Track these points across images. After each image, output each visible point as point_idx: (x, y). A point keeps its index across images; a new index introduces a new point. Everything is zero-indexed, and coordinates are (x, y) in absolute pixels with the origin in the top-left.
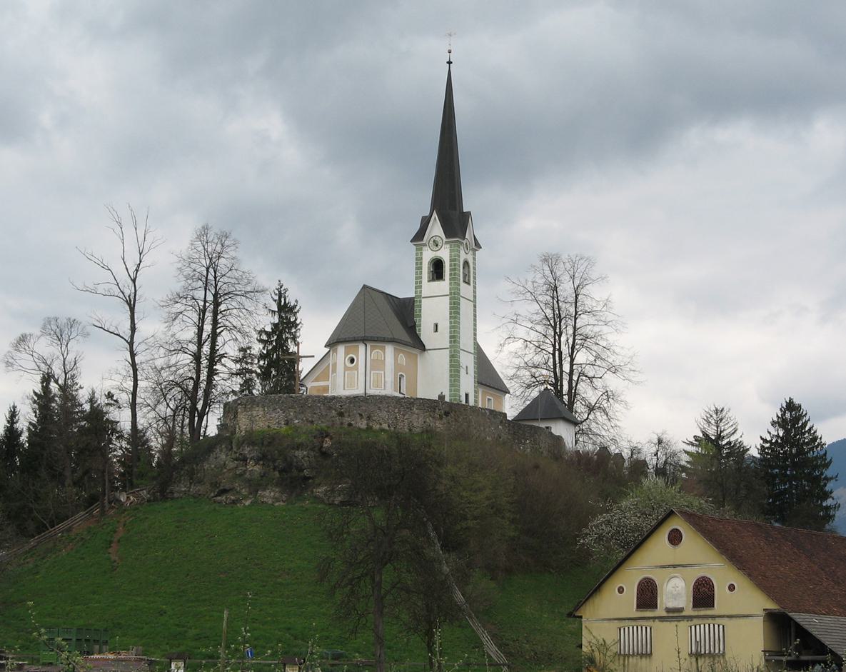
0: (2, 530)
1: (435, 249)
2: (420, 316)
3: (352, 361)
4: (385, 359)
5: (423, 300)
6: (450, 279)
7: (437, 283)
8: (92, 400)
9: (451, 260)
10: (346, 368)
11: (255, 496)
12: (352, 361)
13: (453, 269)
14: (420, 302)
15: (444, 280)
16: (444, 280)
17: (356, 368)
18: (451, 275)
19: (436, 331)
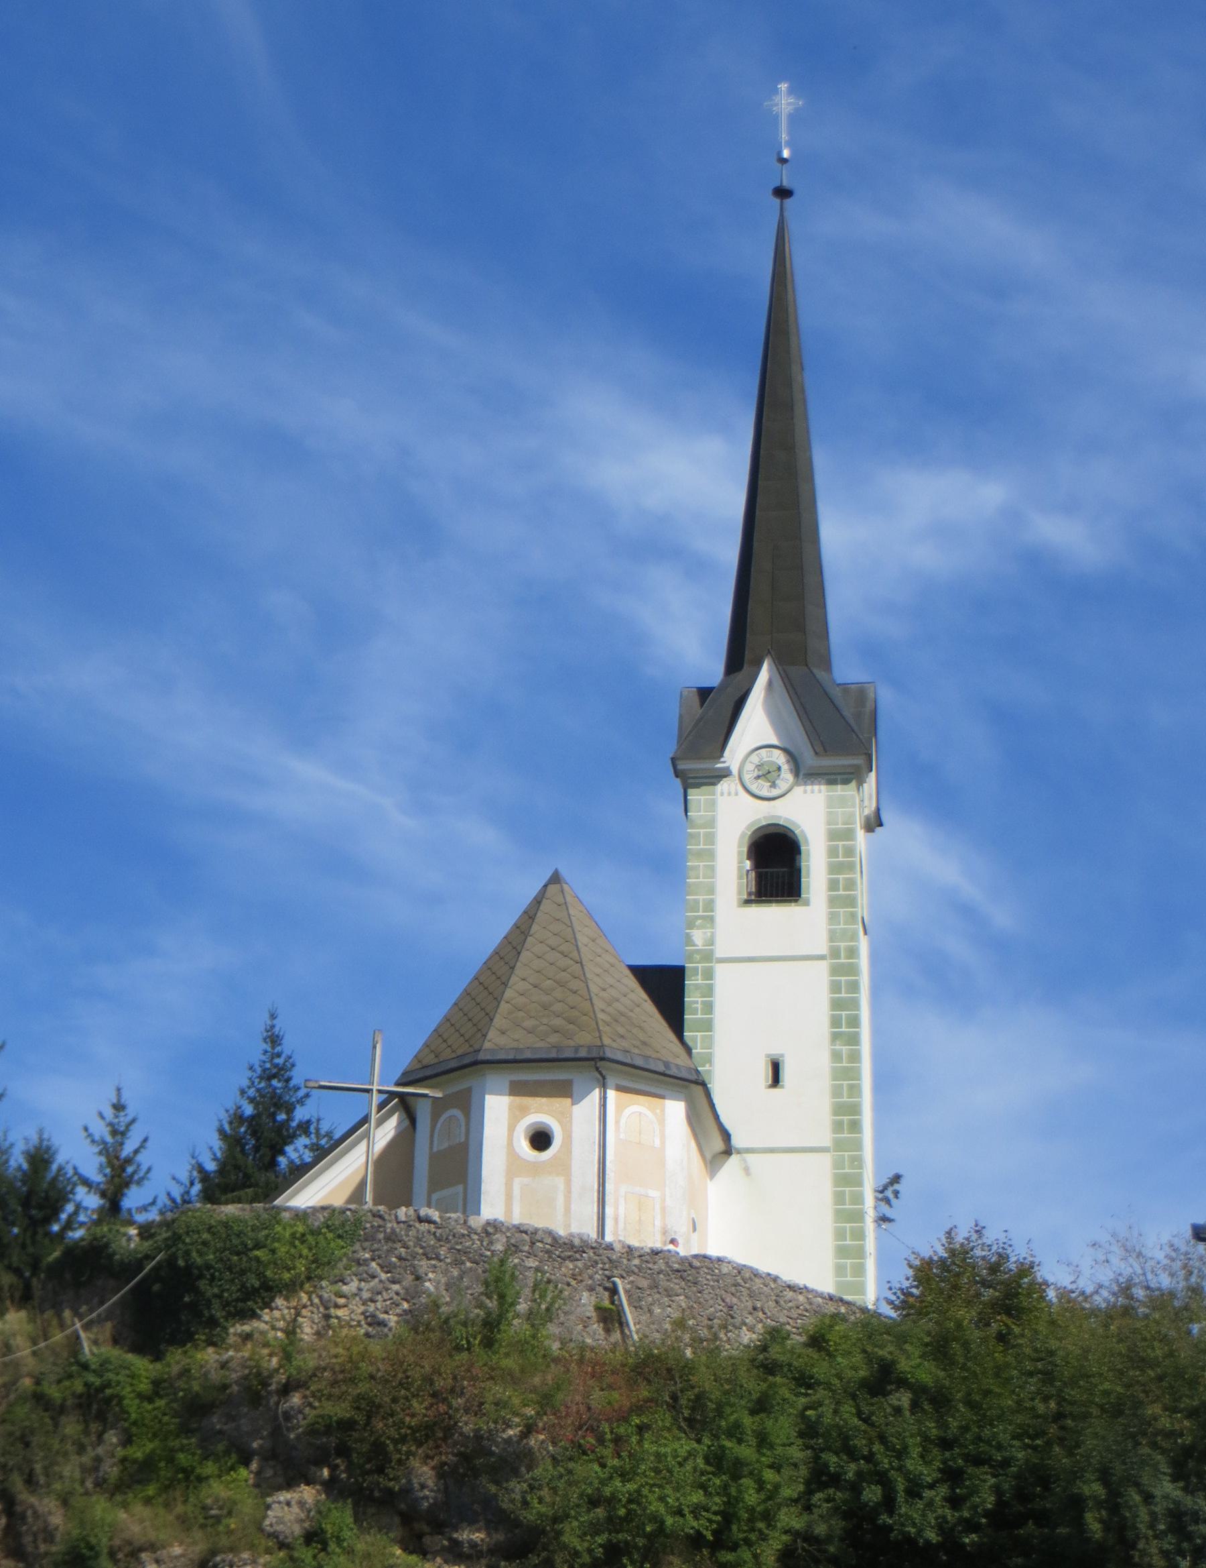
0: (1192, 1414)
1: (765, 793)
2: (708, 1026)
3: (541, 1140)
4: (663, 1142)
5: (720, 970)
6: (833, 901)
7: (775, 913)
8: (60, 1169)
9: (833, 835)
10: (515, 1165)
11: (579, 1482)
12: (541, 1140)
13: (841, 866)
14: (709, 974)
15: (807, 903)
16: (807, 903)
17: (563, 1167)
18: (833, 885)
19: (776, 1080)
